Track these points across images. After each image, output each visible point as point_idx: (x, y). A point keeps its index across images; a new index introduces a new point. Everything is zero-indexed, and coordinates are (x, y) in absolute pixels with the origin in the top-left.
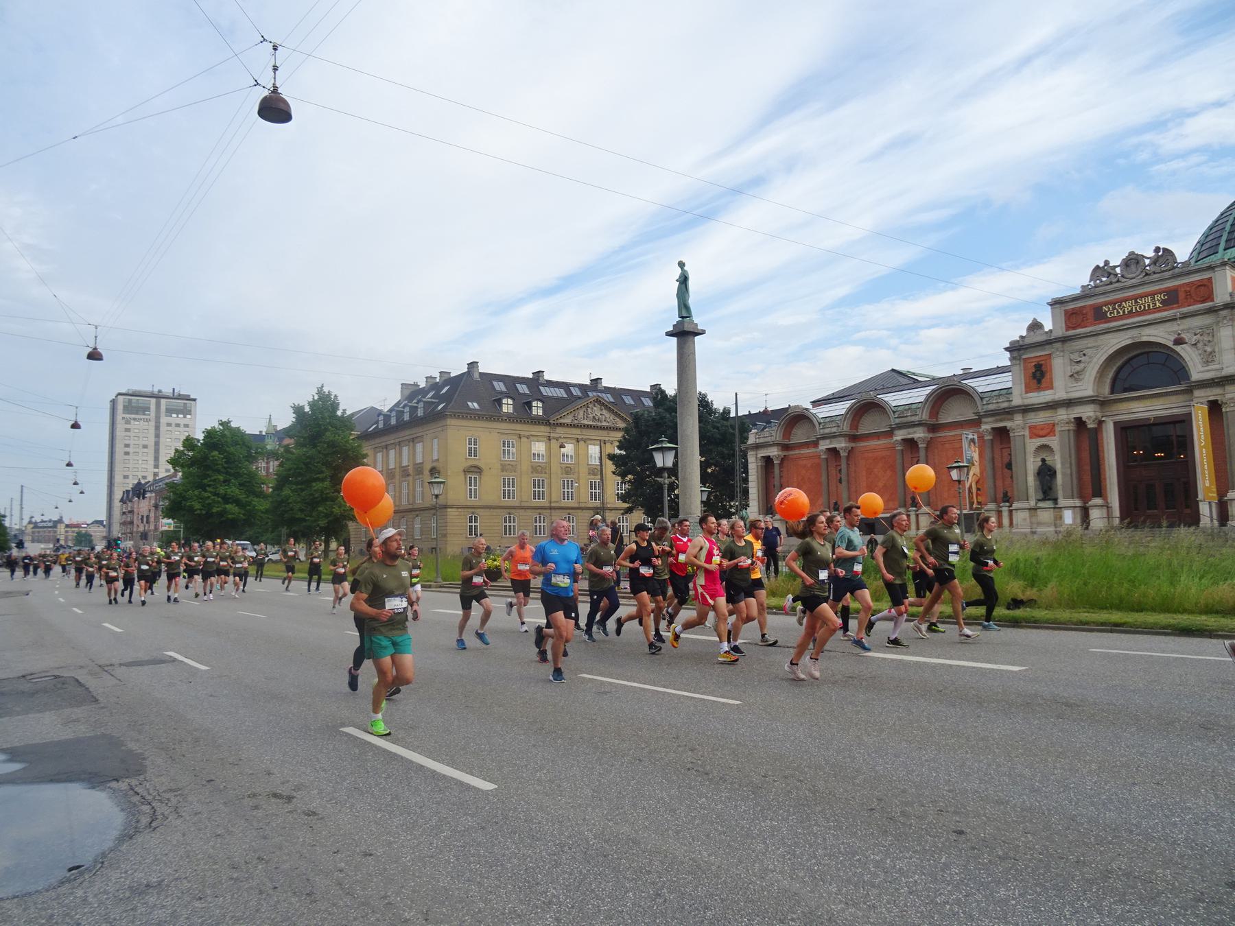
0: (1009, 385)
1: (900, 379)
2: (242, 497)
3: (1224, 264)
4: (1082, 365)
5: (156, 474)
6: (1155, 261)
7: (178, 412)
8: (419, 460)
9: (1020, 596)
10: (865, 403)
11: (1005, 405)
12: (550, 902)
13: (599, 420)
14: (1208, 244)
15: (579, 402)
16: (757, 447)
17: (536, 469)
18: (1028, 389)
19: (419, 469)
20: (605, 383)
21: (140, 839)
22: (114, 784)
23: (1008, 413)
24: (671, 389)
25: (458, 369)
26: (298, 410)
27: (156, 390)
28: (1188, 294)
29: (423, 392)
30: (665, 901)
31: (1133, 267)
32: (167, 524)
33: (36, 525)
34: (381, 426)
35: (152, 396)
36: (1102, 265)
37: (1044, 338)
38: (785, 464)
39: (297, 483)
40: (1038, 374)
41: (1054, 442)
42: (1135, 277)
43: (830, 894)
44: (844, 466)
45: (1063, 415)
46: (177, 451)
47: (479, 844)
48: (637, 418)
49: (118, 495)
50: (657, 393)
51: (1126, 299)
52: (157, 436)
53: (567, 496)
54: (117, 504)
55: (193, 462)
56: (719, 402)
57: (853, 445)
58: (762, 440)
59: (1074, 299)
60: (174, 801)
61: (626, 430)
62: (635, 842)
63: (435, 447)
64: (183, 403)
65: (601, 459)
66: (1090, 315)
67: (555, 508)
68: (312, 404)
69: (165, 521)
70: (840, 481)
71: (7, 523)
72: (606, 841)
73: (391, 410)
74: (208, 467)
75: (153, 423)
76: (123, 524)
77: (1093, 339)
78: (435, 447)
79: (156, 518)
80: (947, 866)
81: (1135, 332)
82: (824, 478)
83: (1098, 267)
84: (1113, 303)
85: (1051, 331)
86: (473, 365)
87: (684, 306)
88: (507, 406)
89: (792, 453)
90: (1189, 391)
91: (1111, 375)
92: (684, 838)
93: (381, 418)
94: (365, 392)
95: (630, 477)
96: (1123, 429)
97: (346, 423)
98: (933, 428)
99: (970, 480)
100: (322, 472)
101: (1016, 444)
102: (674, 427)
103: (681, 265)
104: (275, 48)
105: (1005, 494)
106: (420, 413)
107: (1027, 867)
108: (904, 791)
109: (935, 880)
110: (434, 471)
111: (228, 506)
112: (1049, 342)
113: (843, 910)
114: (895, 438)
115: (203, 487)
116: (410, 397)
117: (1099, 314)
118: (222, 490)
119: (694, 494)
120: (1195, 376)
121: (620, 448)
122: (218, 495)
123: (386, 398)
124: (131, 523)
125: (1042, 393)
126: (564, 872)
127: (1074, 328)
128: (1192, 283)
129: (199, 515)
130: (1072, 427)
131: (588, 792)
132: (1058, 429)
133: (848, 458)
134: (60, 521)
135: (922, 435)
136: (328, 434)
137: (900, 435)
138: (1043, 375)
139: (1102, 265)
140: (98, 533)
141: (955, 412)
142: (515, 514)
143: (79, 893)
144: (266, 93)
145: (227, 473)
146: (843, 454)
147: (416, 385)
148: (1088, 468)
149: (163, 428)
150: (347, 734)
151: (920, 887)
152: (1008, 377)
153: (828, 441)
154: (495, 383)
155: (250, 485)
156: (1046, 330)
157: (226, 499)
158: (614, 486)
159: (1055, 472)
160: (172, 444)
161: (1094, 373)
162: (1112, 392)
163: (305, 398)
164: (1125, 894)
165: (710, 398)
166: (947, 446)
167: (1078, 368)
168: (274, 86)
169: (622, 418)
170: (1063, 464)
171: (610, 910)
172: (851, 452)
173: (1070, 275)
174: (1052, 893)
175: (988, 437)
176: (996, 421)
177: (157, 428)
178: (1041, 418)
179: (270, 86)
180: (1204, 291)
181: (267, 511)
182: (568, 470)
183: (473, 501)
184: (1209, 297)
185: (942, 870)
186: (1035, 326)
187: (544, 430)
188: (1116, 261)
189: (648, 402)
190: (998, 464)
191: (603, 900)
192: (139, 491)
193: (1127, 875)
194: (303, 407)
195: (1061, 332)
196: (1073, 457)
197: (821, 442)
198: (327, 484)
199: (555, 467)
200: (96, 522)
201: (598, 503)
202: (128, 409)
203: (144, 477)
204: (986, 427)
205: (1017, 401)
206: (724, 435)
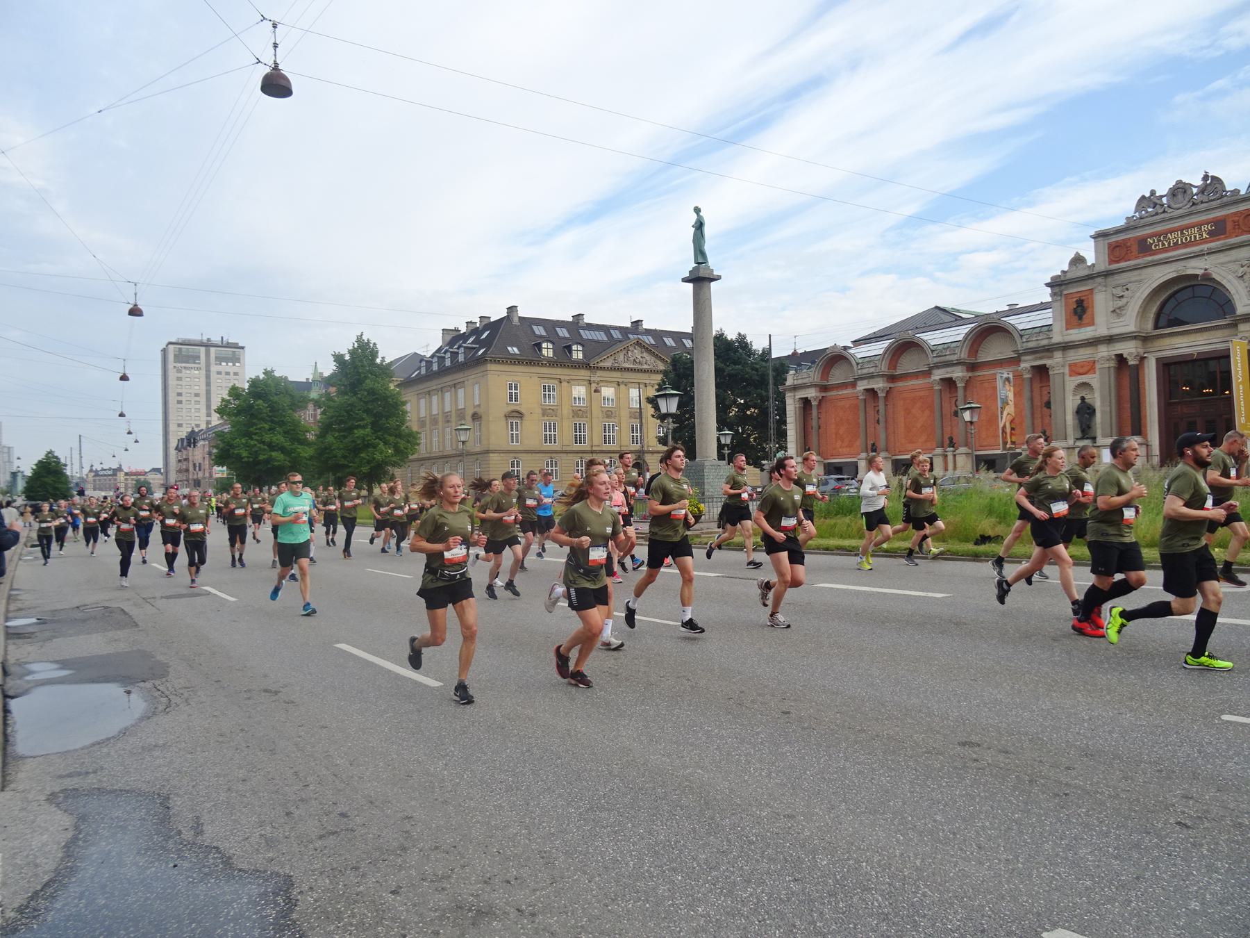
1: (942, 317)
2: (287, 444)
4: (1124, 301)
5: (208, 423)
6: (1202, 190)
7: (227, 360)
8: (461, 406)
9: (991, 533)
10: (903, 343)
11: (1045, 342)
13: (640, 363)
16: (795, 388)
17: (577, 413)
18: (1069, 326)
19: (461, 415)
21: (155, 719)
22: (142, 684)
23: (1048, 350)
25: (497, 313)
26: (338, 358)
27: (205, 339)
28: (1236, 224)
29: (464, 337)
31: (1180, 196)
32: (221, 472)
33: (96, 473)
34: (423, 371)
35: (201, 344)
36: (1147, 195)
37: (1086, 272)
38: (823, 405)
39: (339, 431)
40: (1079, 310)
41: (1094, 379)
42: (1183, 206)
45: (1104, 352)
46: (223, 400)
49: (173, 443)
51: (1171, 231)
52: (208, 384)
53: (608, 440)
54: (172, 452)
55: (239, 412)
57: (970, 374)
58: (800, 382)
60: (186, 695)
61: (665, 373)
63: (477, 392)
64: (232, 352)
66: (1135, 248)
68: (352, 352)
69: (217, 468)
70: (878, 422)
71: (68, 472)
73: (432, 356)
74: (253, 416)
75: (203, 372)
76: (180, 471)
77: (1136, 272)
78: (477, 392)
79: (211, 466)
81: (1174, 266)
82: (862, 420)
83: (1143, 197)
84: (1158, 235)
85: (1093, 265)
86: (512, 309)
87: (700, 252)
88: (547, 350)
89: (829, 394)
90: (1234, 325)
91: (1154, 309)
93: (423, 364)
94: (407, 338)
96: (1167, 367)
97: (385, 371)
98: (973, 367)
99: (1004, 420)
100: (363, 419)
101: (1055, 381)
103: (697, 210)
104: (275, 26)
105: (951, 440)
106: (461, 358)
110: (476, 417)
111: (274, 454)
112: (1091, 277)
115: (249, 435)
116: (451, 343)
117: (1144, 247)
118: (267, 438)
122: (263, 443)
123: (429, 343)
124: (187, 470)
125: (1083, 330)
127: (1118, 262)
128: (1241, 212)
129: (247, 463)
130: (1113, 364)
132: (1098, 366)
133: (886, 398)
134: (120, 469)
135: (960, 375)
136: (368, 381)
137: (938, 375)
138: (1084, 311)
139: (1147, 195)
140: (156, 480)
141: (994, 350)
142: (557, 457)
143: (105, 750)
144: (268, 70)
145: (272, 421)
146: (881, 395)
147: (457, 330)
149: (213, 376)
152: (1048, 313)
153: (865, 382)
154: (535, 328)
155: (295, 433)
156: (1089, 264)
157: (272, 447)
159: (1094, 410)
160: (220, 394)
161: (1137, 308)
162: (1156, 327)
163: (345, 346)
165: (749, 339)
166: (986, 385)
168: (275, 63)
170: (1102, 402)
172: (889, 391)
173: (1115, 203)
176: (1035, 359)
177: (208, 377)
179: (271, 63)
181: (311, 458)
182: (609, 414)
183: (515, 445)
186: (1078, 260)
187: (583, 374)
188: (1162, 190)
190: (1037, 402)
192: (191, 440)
194: (342, 356)
195: (1104, 266)
196: (1113, 394)
198: (368, 430)
199: (596, 411)
200: (154, 470)
202: (179, 357)
203: (198, 426)
204: (1026, 364)
205: (1057, 338)
206: (749, 379)
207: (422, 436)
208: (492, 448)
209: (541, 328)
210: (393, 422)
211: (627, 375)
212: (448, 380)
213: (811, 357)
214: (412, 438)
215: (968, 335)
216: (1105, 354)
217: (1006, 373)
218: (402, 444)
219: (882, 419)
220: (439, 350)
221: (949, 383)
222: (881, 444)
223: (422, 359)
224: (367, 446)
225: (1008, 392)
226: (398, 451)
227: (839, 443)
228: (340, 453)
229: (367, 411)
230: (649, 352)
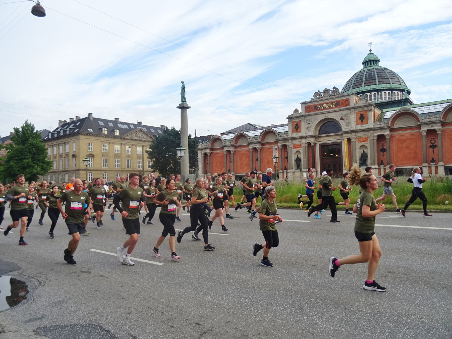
4: (310, 125)
6: (333, 92)
8: (67, 151)
10: (240, 135)
11: (286, 137)
16: (202, 149)
17: (116, 156)
18: (294, 132)
19: (67, 155)
23: (287, 140)
25: (83, 115)
28: (342, 103)
29: (69, 124)
31: (326, 93)
34: (50, 137)
37: (299, 115)
38: (212, 155)
39: (16, 160)
41: (301, 150)
45: (304, 141)
51: (324, 104)
58: (203, 147)
63: (74, 146)
66: (313, 108)
68: (23, 128)
70: (231, 162)
73: (54, 131)
78: (74, 146)
82: (225, 161)
86: (90, 114)
87: (183, 98)
88: (105, 131)
89: (214, 152)
90: (342, 135)
93: (50, 134)
96: (323, 147)
97: (38, 135)
98: (263, 144)
100: (27, 155)
101: (289, 150)
110: (74, 156)
112: (300, 117)
116: (63, 126)
117: (316, 108)
123: (53, 126)
127: (308, 112)
130: (307, 145)
132: (302, 146)
133: (234, 153)
135: (232, 149)
136: (30, 140)
137: (251, 146)
138: (298, 127)
141: (270, 139)
146: (232, 152)
147: (65, 121)
152: (287, 127)
153: (227, 148)
154: (99, 122)
161: (314, 128)
162: (319, 134)
168: (38, 2)
178: (297, 142)
182: (129, 156)
184: (348, 105)
186: (296, 111)
187: (119, 141)
190: (283, 157)
194: (18, 129)
195: (304, 113)
198: (30, 160)
199: (124, 156)
204: (280, 144)
205: (290, 136)
207: (55, 162)
208: (81, 168)
209: (111, 124)
210: (41, 157)
211: (136, 142)
212: (61, 141)
213: (208, 138)
214: (49, 164)
215: (262, 133)
216: (304, 142)
217: (275, 147)
218: (45, 166)
219: (232, 161)
220: (57, 129)
221: (255, 149)
222: (232, 170)
223: (49, 132)
224: (29, 166)
225: (276, 153)
226: (43, 168)
227: (217, 169)
228: (16, 169)
229: (30, 152)
230: (144, 133)
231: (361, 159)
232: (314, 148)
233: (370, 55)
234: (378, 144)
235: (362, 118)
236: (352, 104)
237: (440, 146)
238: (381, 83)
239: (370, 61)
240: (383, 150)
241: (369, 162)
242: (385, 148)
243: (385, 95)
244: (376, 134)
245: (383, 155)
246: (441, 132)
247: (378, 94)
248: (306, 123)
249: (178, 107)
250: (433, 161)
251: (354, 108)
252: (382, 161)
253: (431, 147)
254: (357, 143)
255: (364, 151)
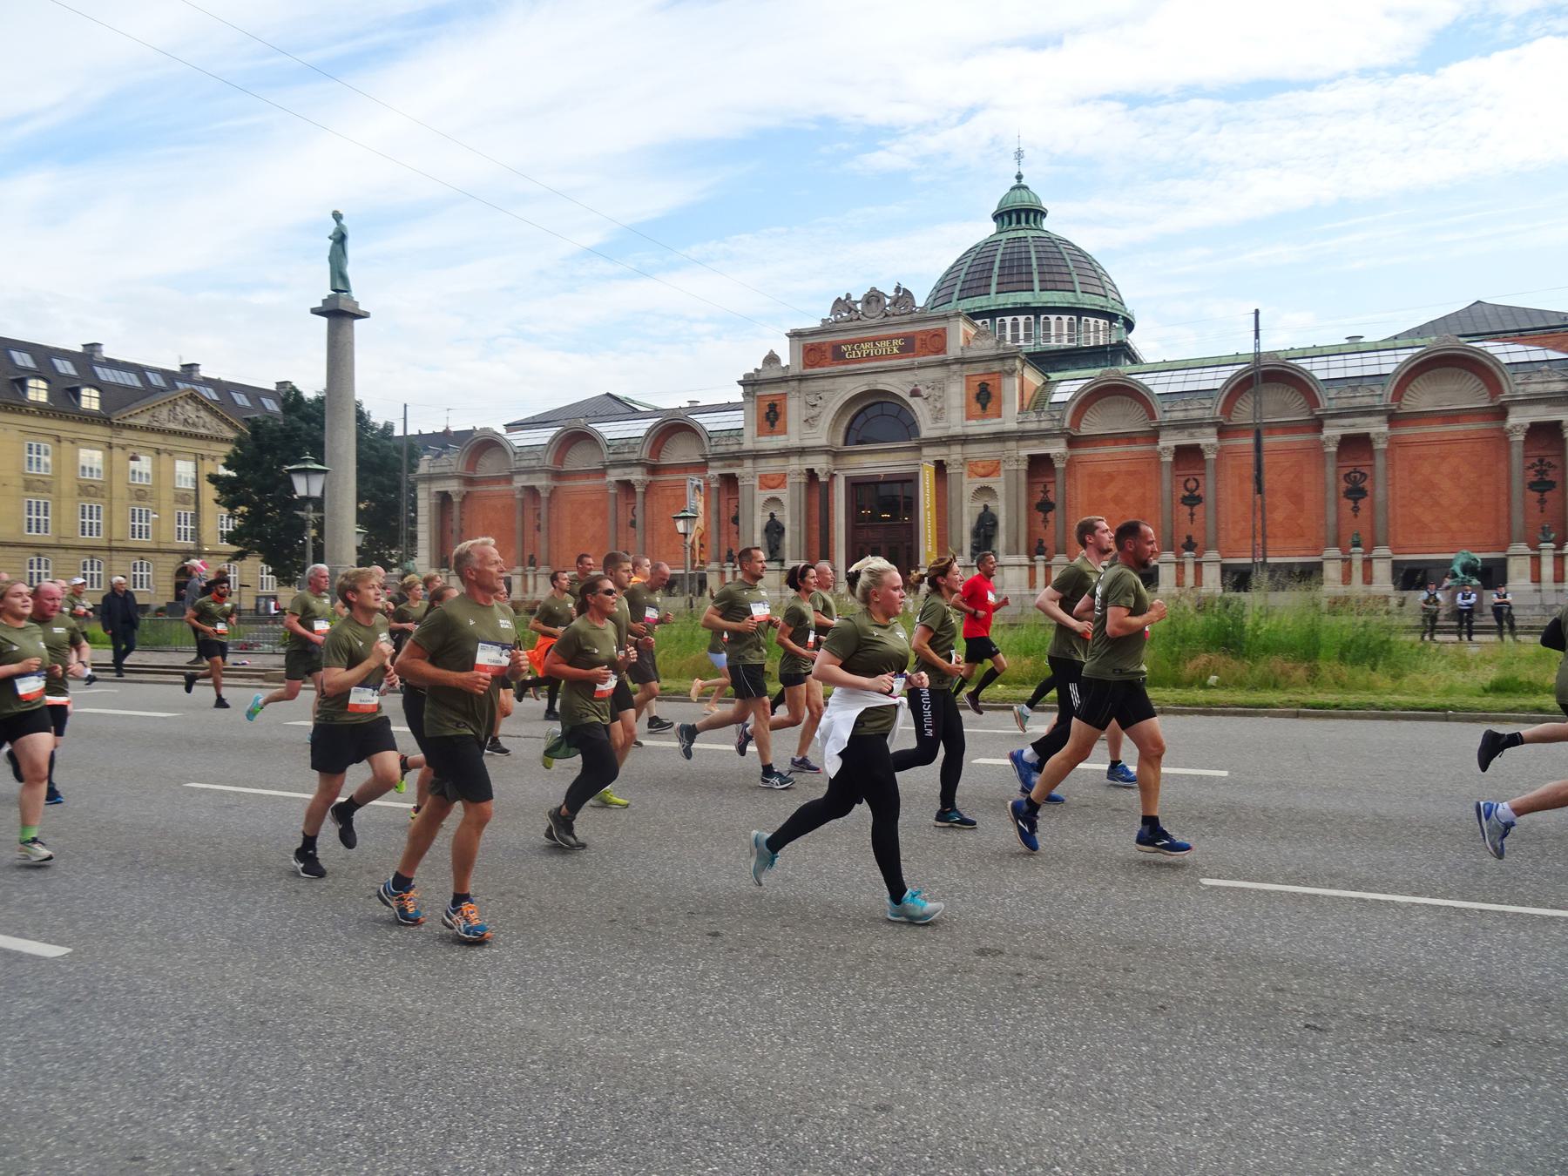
0: (741, 425)
3: (958, 315)
4: (817, 410)
10: (574, 433)
11: (735, 448)
12: (186, 1097)
13: (194, 425)
14: (943, 291)
15: (164, 395)
16: (430, 478)
17: (86, 490)
20: (204, 372)
23: (738, 458)
24: (312, 385)
30: (360, 1067)
31: (874, 305)
37: (780, 374)
41: (784, 494)
43: (575, 1024)
44: (544, 505)
45: (796, 465)
47: (52, 1035)
48: (255, 426)
50: (289, 397)
51: (864, 341)
56: (378, 418)
58: (438, 470)
59: (814, 333)
62: (306, 999)
65: (196, 482)
66: (829, 355)
67: (118, 550)
72: (263, 1004)
80: (705, 973)
81: (871, 378)
84: (852, 343)
88: (38, 392)
90: (918, 449)
91: (845, 423)
92: (376, 984)
95: (243, 509)
96: (855, 485)
98: (654, 470)
101: (744, 494)
102: (322, 445)
107: (789, 962)
108: (648, 896)
109: (695, 991)
112: (784, 380)
113: (594, 1041)
114: (608, 479)
119: (347, 536)
120: (926, 432)
121: (227, 466)
126: (201, 1054)
127: (812, 366)
130: (803, 479)
131: (225, 942)
132: (789, 480)
133: (549, 499)
135: (640, 477)
138: (777, 416)
146: (544, 494)
148: (816, 526)
150: (60, 943)
151: (678, 1001)
153: (524, 477)
158: (218, 521)
161: (829, 420)
162: (846, 444)
164: (885, 977)
167: (814, 412)
169: (231, 425)
171: (281, 1091)
172: (466, 497)
174: (817, 986)
175: (714, 485)
176: (724, 467)
178: (771, 466)
180: (937, 341)
182: (140, 495)
184: (942, 349)
185: (701, 978)
186: (772, 359)
189: (272, 406)
190: (724, 517)
191: (268, 1081)
193: (886, 956)
195: (797, 369)
197: (516, 478)
199: (119, 489)
201: (190, 544)
204: (714, 471)
205: (748, 444)
206: (387, 463)
231: (976, 533)
232: (827, 488)
233: (1018, 192)
234: (1030, 484)
235: (985, 397)
236: (955, 347)
237: (1209, 498)
238: (1049, 285)
239: (1018, 212)
240: (1046, 506)
241: (1001, 541)
242: (1052, 499)
243: (1059, 327)
244: (1024, 453)
245: (1356, 509)
246: (1385, 446)
247: (1079, 320)
248: (803, 404)
249: (315, 311)
250: (1190, 545)
251: (961, 361)
252: (1041, 542)
253: (1185, 500)
254: (965, 479)
255: (986, 507)
